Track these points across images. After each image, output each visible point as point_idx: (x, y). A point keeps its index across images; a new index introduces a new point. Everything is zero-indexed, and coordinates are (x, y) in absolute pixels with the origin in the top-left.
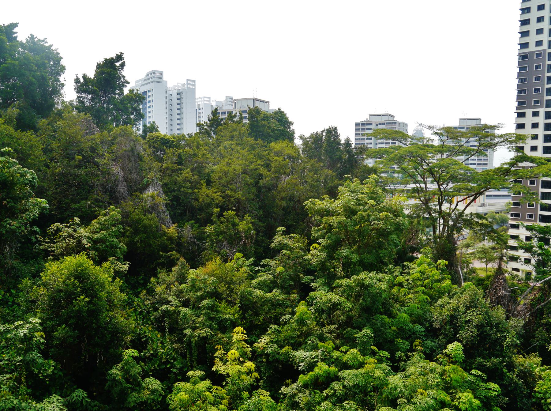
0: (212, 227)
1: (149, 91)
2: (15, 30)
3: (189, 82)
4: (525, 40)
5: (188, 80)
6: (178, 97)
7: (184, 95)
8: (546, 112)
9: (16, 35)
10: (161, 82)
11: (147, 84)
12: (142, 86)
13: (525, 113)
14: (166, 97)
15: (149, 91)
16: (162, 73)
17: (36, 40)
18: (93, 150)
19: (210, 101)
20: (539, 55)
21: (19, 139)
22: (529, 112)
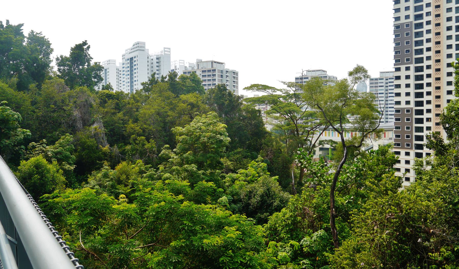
0: (130, 146)
1: (135, 57)
2: (21, 28)
3: (166, 50)
4: (398, 15)
5: (165, 48)
6: (158, 61)
7: (162, 60)
8: (415, 67)
9: (22, 31)
10: (143, 50)
11: (134, 52)
12: (130, 53)
13: (400, 68)
14: (148, 62)
15: (135, 57)
16: (144, 43)
17: (35, 34)
18: (63, 101)
19: (184, 63)
20: (407, 25)
21: (16, 96)
22: (403, 67)
